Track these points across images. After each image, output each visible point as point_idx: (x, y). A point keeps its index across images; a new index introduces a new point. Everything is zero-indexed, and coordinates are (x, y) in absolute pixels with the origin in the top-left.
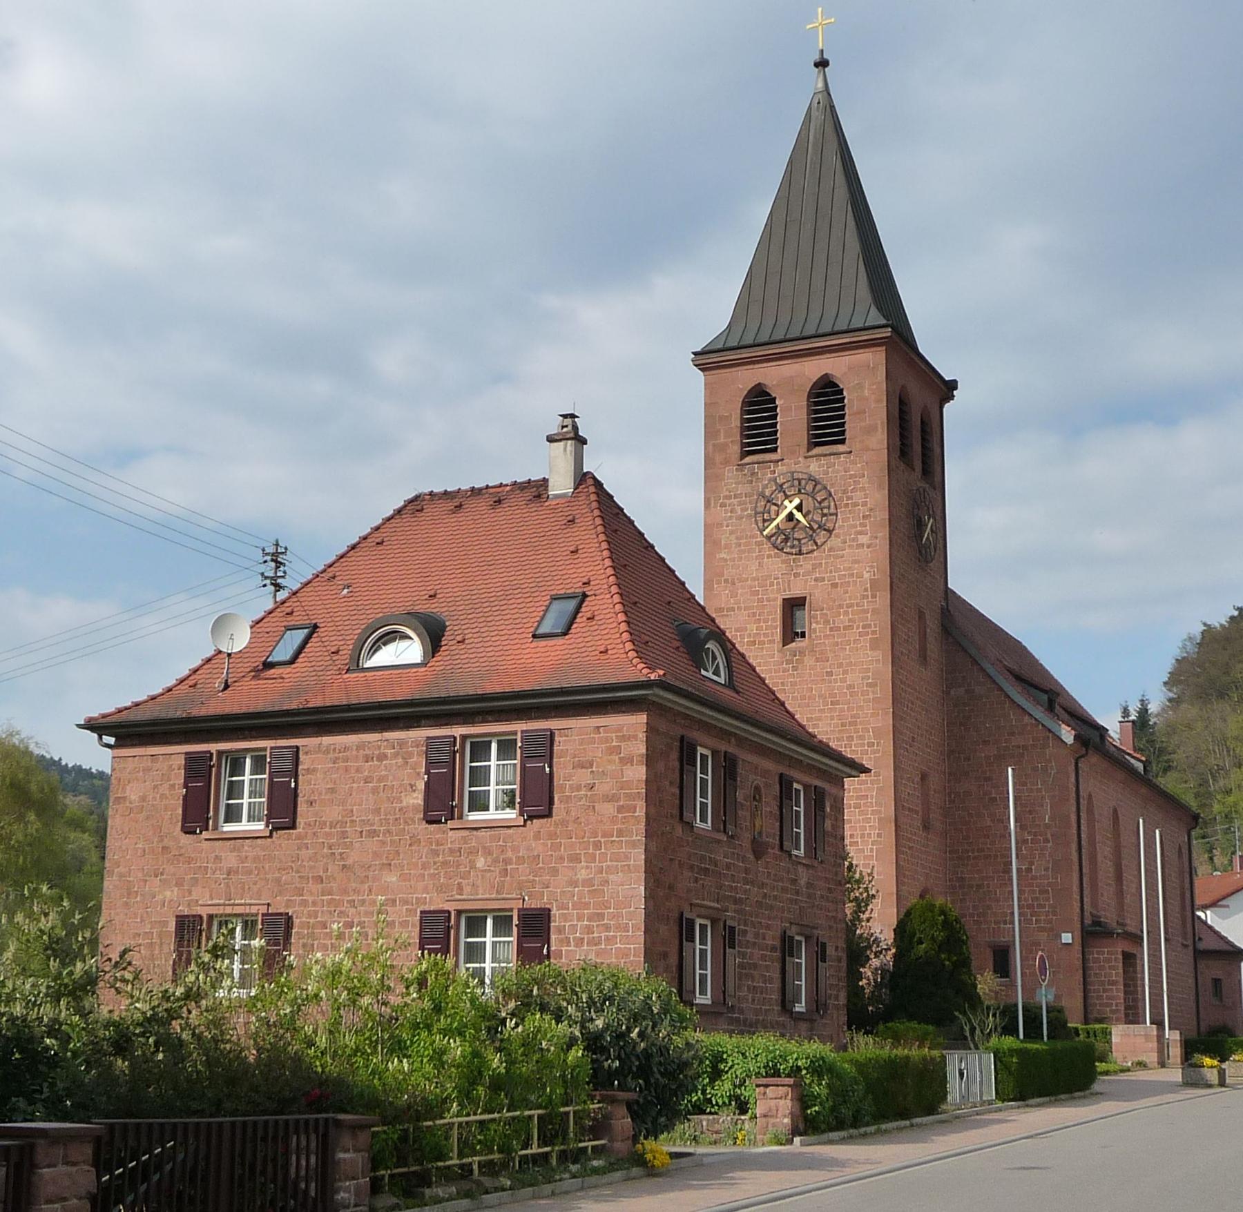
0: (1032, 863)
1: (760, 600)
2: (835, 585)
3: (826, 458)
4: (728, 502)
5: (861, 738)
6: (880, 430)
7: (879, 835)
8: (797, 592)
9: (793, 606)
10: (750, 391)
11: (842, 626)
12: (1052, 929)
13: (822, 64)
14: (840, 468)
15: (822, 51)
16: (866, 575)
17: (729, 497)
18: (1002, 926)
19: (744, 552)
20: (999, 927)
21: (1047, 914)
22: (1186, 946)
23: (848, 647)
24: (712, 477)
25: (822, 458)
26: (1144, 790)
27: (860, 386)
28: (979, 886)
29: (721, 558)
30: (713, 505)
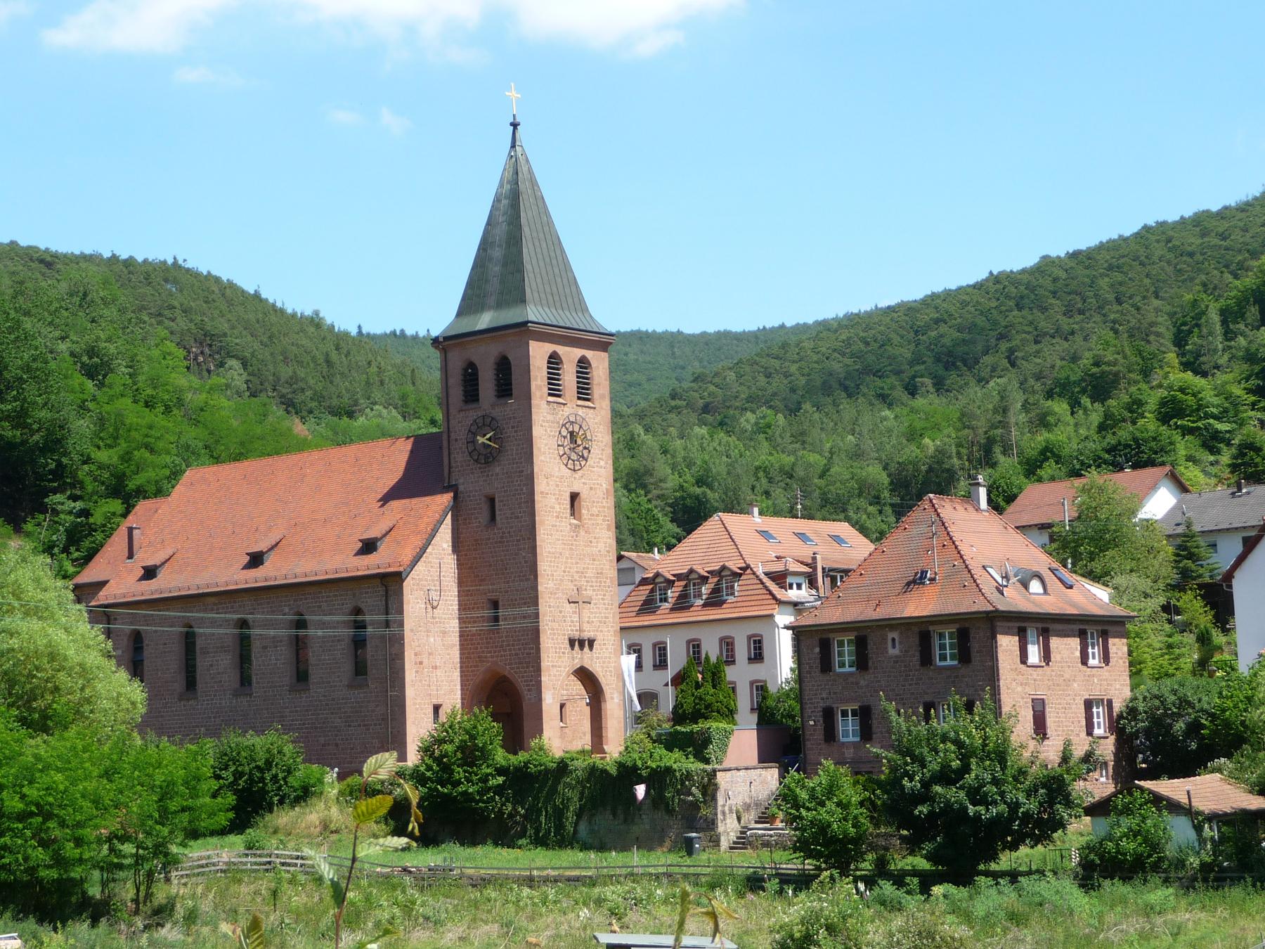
9: (574, 497)
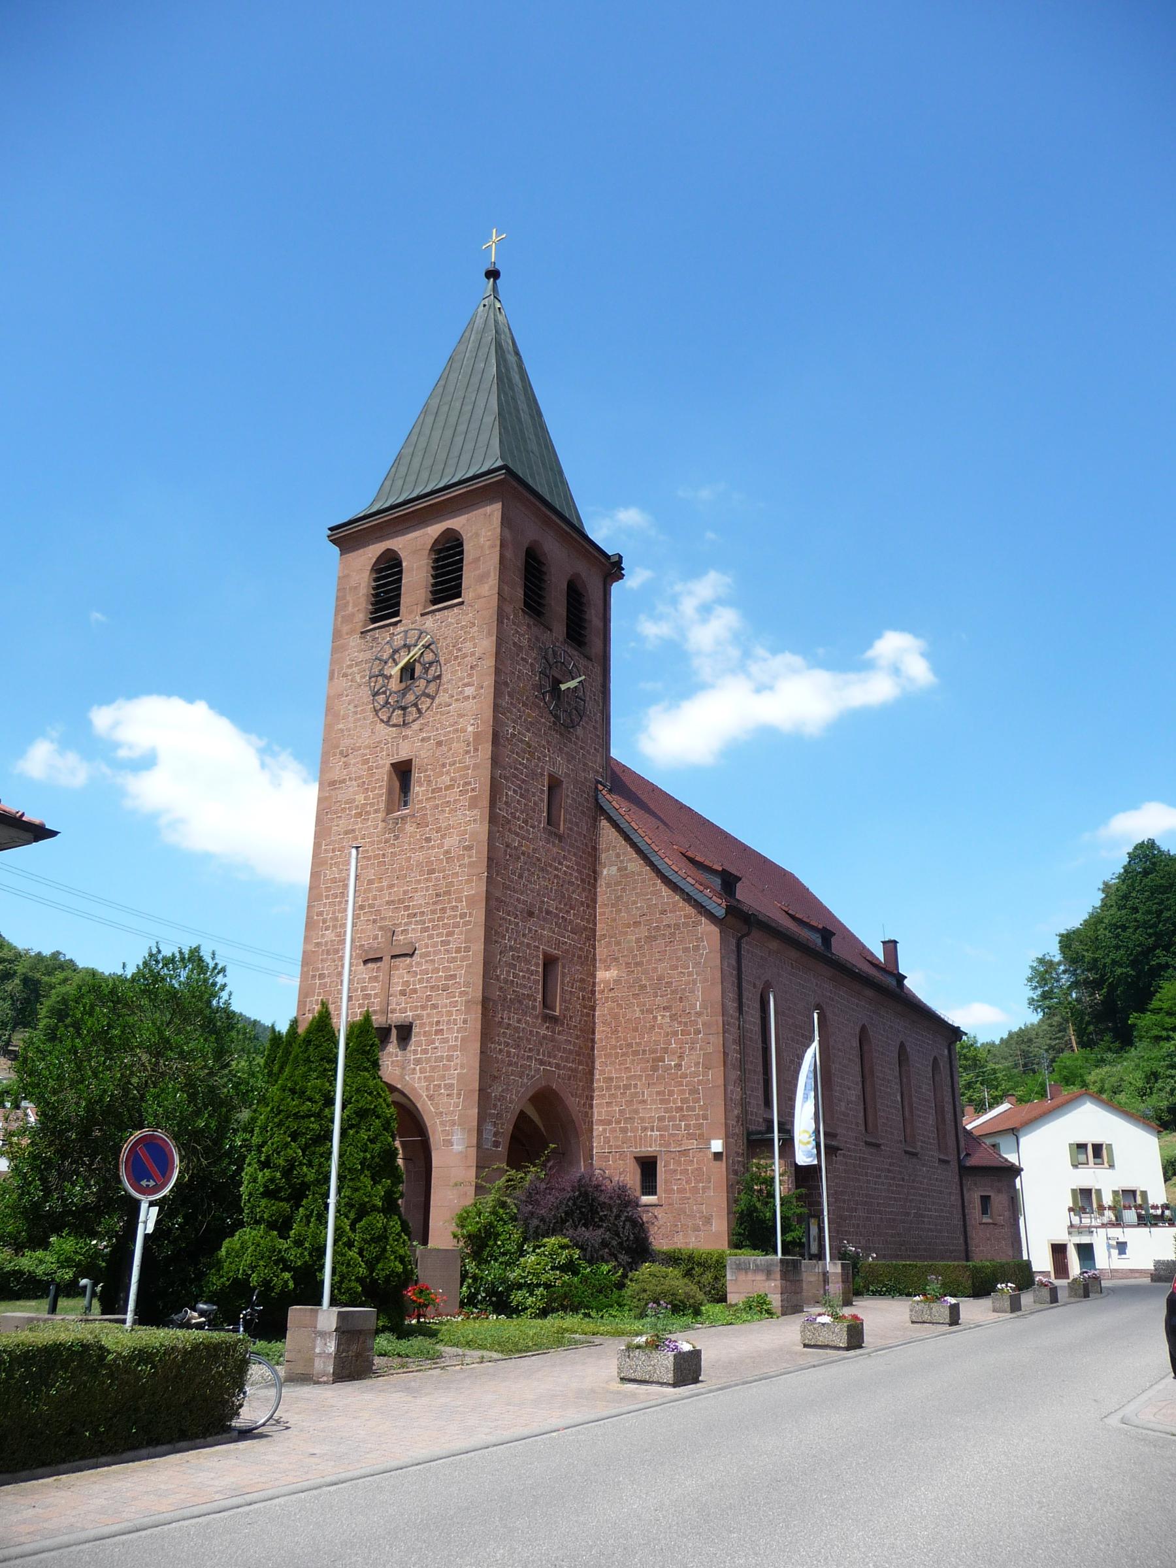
0: (681, 1057)
1: (370, 769)
2: (439, 744)
3: (440, 613)
4: (350, 671)
5: (454, 908)
6: (492, 574)
7: (465, 1022)
8: (403, 755)
9: (403, 772)
10: (378, 559)
11: (443, 786)
12: (701, 1136)
13: (493, 274)
14: (453, 620)
15: (495, 263)
16: (470, 729)
17: (350, 666)
18: (649, 1133)
19: (359, 719)
20: (646, 1135)
21: (697, 1117)
22: (946, 1162)
23: (448, 809)
24: (338, 648)
25: (437, 613)
26: (869, 993)
27: (477, 535)
28: (627, 1087)
29: (338, 730)
30: (336, 676)
